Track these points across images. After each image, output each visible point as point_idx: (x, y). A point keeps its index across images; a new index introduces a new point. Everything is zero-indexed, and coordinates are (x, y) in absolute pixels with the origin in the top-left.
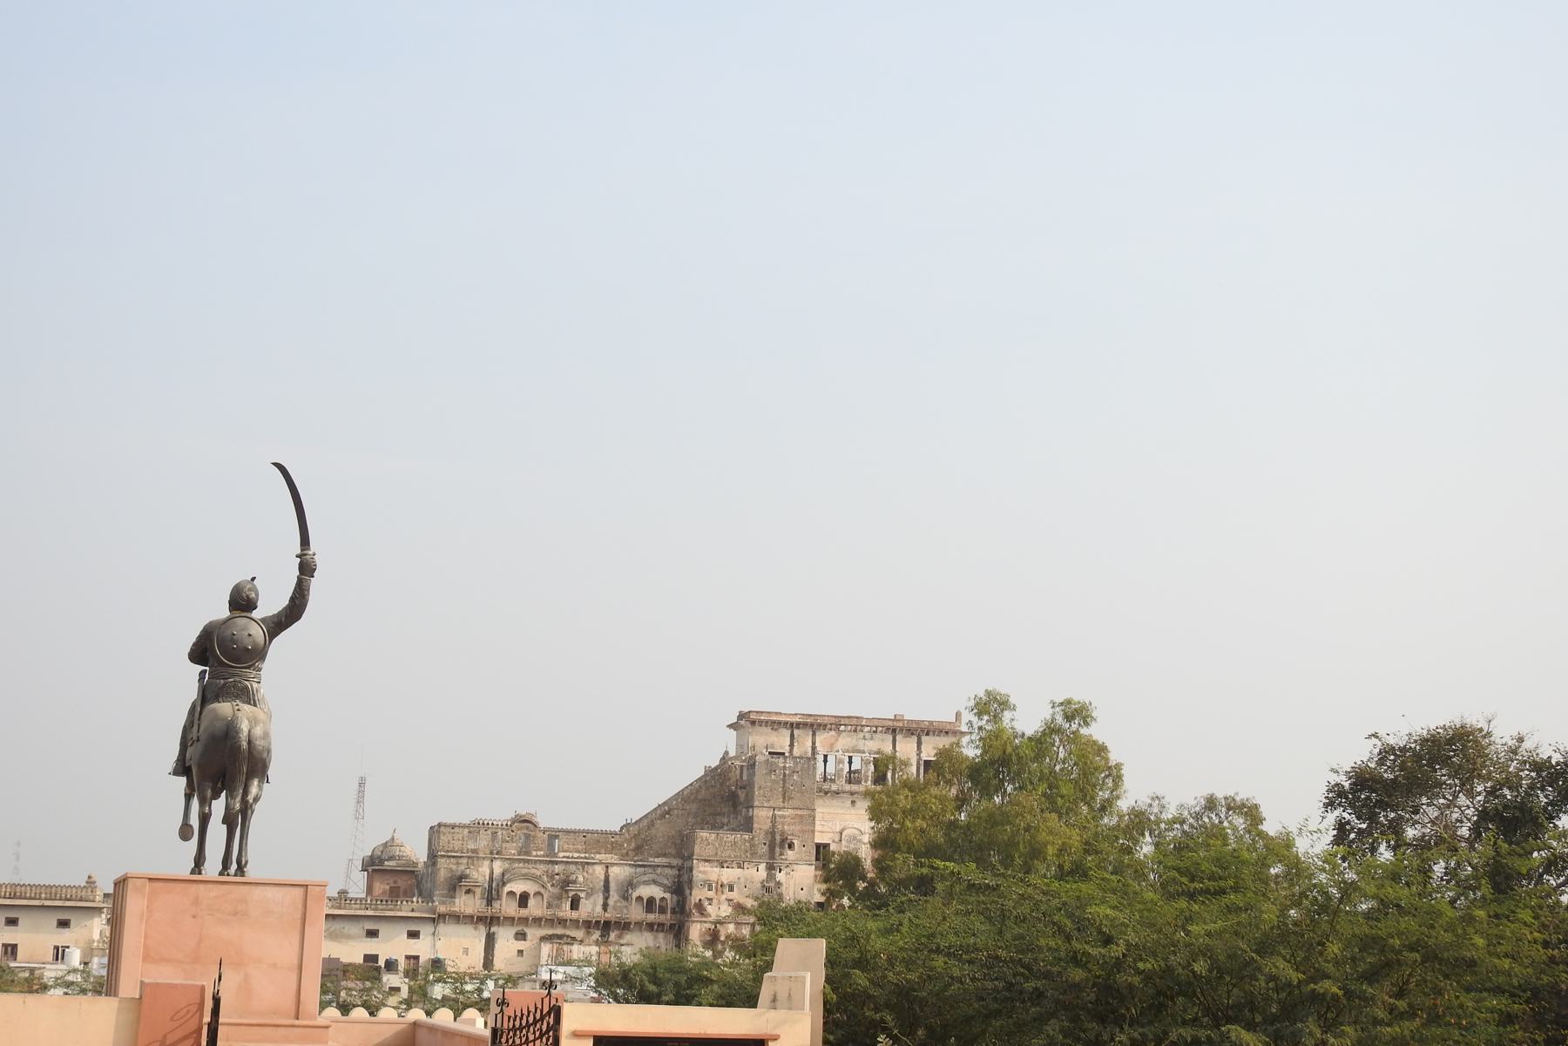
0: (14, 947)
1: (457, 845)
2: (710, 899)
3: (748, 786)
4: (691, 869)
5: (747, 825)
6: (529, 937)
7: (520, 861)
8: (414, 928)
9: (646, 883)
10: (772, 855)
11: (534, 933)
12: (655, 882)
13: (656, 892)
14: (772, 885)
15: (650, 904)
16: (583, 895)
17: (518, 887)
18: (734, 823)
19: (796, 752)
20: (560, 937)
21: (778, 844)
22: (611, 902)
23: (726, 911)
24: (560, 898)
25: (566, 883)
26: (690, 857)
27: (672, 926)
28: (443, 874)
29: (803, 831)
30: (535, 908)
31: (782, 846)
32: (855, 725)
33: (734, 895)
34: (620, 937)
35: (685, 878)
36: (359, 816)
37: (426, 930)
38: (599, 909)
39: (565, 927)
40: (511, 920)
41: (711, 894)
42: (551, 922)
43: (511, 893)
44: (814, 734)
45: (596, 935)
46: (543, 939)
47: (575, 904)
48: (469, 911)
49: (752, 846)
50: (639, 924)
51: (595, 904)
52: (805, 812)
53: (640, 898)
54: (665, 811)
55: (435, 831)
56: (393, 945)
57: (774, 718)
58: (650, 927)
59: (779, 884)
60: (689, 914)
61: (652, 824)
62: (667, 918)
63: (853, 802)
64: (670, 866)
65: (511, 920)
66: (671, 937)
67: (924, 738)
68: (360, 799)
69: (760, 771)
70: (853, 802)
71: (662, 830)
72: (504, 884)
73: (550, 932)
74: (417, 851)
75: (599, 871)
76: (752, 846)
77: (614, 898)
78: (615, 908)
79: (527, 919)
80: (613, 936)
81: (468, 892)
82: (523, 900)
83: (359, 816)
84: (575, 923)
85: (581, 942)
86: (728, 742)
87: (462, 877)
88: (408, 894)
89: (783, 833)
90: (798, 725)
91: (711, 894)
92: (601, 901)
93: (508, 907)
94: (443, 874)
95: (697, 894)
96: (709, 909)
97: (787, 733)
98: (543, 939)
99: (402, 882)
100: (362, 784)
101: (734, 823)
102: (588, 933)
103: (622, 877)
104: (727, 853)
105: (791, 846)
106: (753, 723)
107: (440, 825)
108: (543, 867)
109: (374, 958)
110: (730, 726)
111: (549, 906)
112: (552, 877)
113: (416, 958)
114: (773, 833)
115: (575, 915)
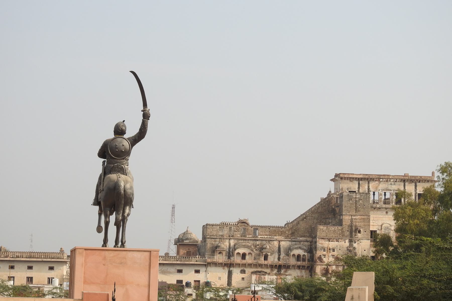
0: (32, 278)
1: (215, 233)
2: (325, 255)
3: (340, 206)
4: (316, 242)
5: (340, 223)
6: (247, 272)
8: (197, 268)
11: (249, 270)
12: (300, 248)
13: (300, 252)
14: (352, 249)
16: (269, 254)
18: (334, 222)
19: (361, 191)
20: (260, 272)
21: (354, 231)
22: (281, 257)
23: (331, 259)
24: (259, 255)
25: (262, 249)
26: (315, 237)
27: (308, 267)
29: (365, 225)
30: (249, 259)
31: (355, 232)
32: (387, 178)
33: (335, 253)
34: (286, 272)
36: (172, 221)
37: (202, 269)
38: (276, 260)
39: (262, 268)
40: (239, 265)
42: (256, 265)
43: (238, 254)
44: (369, 183)
45: (275, 271)
46: (253, 273)
47: (266, 258)
48: (220, 261)
49: (343, 232)
50: (294, 266)
51: (274, 258)
52: (366, 217)
53: (294, 255)
54: (304, 217)
55: (205, 227)
57: (351, 176)
58: (299, 267)
59: (355, 248)
60: (316, 262)
61: (298, 223)
62: (306, 263)
63: (387, 212)
64: (307, 241)
65: (239, 265)
67: (418, 184)
69: (345, 199)
70: (387, 212)
71: (303, 226)
72: (235, 250)
73: (256, 270)
74: (198, 236)
75: (276, 243)
76: (343, 232)
78: (283, 259)
79: (245, 264)
80: (282, 271)
81: (220, 253)
82: (244, 256)
83: (172, 221)
84: (266, 266)
85: (269, 274)
86: (331, 187)
87: (217, 247)
88: (194, 254)
89: (356, 226)
90: (361, 179)
92: (277, 256)
93: (238, 260)
94: (209, 246)
95: (319, 253)
97: (357, 182)
98: (253, 273)
99: (192, 249)
100: (173, 208)
101: (334, 222)
102: (272, 270)
103: (286, 246)
104: (332, 235)
105: (359, 232)
106: (342, 178)
107: (207, 225)
110: (332, 180)
112: (256, 246)
113: (199, 281)
114: (351, 226)
115: (266, 262)
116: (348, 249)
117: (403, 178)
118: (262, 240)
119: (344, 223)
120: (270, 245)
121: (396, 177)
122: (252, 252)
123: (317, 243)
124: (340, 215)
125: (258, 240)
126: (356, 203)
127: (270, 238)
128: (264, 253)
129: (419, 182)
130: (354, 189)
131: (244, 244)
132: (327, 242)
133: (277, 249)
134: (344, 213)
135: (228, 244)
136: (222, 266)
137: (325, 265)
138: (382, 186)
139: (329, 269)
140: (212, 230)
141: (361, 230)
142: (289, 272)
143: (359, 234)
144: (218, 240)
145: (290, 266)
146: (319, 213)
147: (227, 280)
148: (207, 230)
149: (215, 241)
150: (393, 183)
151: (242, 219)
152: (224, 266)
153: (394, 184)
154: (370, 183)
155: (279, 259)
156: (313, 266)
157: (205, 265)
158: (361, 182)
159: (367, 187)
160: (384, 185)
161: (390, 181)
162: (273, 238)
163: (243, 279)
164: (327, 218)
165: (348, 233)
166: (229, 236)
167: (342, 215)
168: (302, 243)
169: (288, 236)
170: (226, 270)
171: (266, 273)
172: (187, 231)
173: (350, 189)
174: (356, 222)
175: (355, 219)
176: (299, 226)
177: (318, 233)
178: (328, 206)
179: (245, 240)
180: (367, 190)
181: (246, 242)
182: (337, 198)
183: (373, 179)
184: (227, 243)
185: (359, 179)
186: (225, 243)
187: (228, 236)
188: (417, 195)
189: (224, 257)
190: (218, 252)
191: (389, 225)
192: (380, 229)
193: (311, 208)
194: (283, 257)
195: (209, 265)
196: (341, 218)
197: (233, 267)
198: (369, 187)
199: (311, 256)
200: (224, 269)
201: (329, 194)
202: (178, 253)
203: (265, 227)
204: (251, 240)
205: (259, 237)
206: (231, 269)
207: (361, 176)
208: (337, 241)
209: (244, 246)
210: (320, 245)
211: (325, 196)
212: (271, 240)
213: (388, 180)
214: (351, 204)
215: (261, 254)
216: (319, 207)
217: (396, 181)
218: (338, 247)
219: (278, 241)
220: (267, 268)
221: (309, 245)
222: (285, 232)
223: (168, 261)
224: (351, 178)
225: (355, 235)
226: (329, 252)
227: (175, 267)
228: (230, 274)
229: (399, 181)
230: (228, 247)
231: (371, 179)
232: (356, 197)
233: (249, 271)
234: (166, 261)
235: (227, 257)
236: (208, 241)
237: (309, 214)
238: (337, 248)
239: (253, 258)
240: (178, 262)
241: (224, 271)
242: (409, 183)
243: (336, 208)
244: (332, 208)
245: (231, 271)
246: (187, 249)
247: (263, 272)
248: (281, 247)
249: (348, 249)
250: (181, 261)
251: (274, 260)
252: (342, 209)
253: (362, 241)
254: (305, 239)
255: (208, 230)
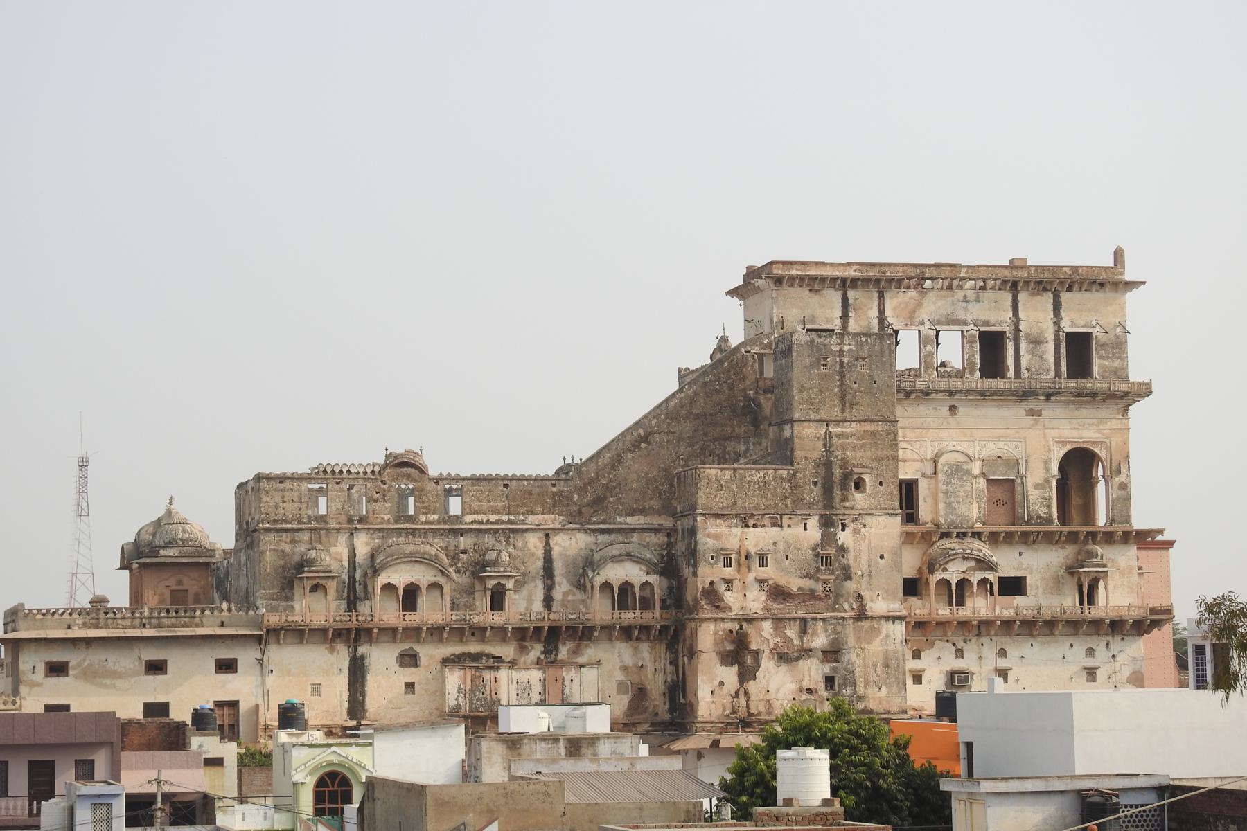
0: (413, 684)
1: (290, 509)
2: (729, 582)
3: (779, 389)
4: (693, 532)
5: (783, 453)
6: (423, 660)
7: (398, 531)
8: (226, 654)
9: (617, 559)
10: (828, 502)
11: (430, 653)
12: (630, 556)
13: (634, 573)
14: (831, 551)
15: (624, 595)
16: (510, 584)
17: (400, 576)
18: (756, 452)
19: (853, 326)
20: (476, 657)
21: (836, 483)
22: (557, 594)
23: (756, 601)
24: (470, 591)
25: (479, 567)
26: (691, 510)
27: (664, 629)
28: (269, 560)
29: (878, 459)
30: (430, 611)
31: (844, 487)
32: (947, 277)
33: (770, 572)
34: (576, 652)
35: (681, 547)
36: (81, 512)
37: (246, 657)
38: (538, 607)
39: (483, 640)
40: (391, 633)
41: (729, 572)
42: (458, 632)
43: (390, 588)
44: (881, 297)
45: (536, 651)
46: (447, 662)
47: (497, 603)
48: (319, 620)
49: (795, 487)
50: (608, 629)
51: (530, 600)
52: (880, 427)
53: (606, 586)
54: (639, 438)
55: (248, 493)
56: (190, 688)
57: (813, 272)
58: (627, 633)
59: (842, 550)
60: (695, 608)
61: (618, 460)
62: (653, 617)
63: (953, 409)
64: (656, 531)
65: (391, 633)
66: (661, 648)
67: (1065, 296)
68: (82, 488)
69: (801, 359)
70: (953, 409)
71: (635, 469)
72: (376, 572)
73: (458, 649)
74: (217, 530)
75: (534, 543)
76: (795, 487)
77: (562, 587)
78: (564, 604)
79: (417, 630)
80: (564, 652)
81: (315, 588)
82: (410, 597)
83: (81, 512)
84: (501, 633)
85: (513, 664)
86: (732, 323)
87: (303, 564)
88: (204, 600)
89: (844, 463)
90: (855, 282)
91: (729, 572)
92: (539, 593)
93: (387, 612)
94: (269, 560)
95: (708, 573)
96: (729, 598)
97: (835, 297)
98: (447, 662)
99: (191, 583)
100: (83, 466)
101: (756, 452)
102: (523, 649)
103: (572, 552)
104: (754, 501)
105: (859, 485)
106: (779, 281)
107: (259, 478)
108: (438, 542)
109: (163, 709)
110: (733, 293)
111: (454, 606)
112: (455, 557)
113: (234, 705)
114: (828, 465)
115: (498, 619)
116: (817, 555)
117: (1007, 273)
118: (479, 531)
119: (798, 453)
120: (511, 550)
121: (984, 274)
122: (441, 580)
123: (700, 536)
124: (780, 425)
125: (462, 533)
126: (842, 375)
127: (510, 522)
128: (490, 584)
129: (1070, 289)
130: (828, 322)
131: (410, 548)
132: (737, 531)
133: (540, 563)
134: (797, 415)
135: (345, 553)
136: (325, 641)
137: (732, 620)
138: (933, 305)
139: (746, 635)
140: (278, 500)
141: (866, 477)
142: (590, 652)
143: (858, 496)
144: (305, 536)
145: (592, 629)
146: (697, 417)
147: (346, 694)
148: (259, 500)
149: (294, 542)
150: (971, 295)
151: (398, 449)
152: (333, 640)
153: (977, 300)
154: (887, 295)
155: (548, 602)
156: (683, 627)
157: (258, 639)
158: (851, 294)
159: (874, 313)
160: (940, 303)
161: (961, 288)
162: (522, 522)
163: (410, 686)
164: (729, 439)
165: (813, 493)
166: (350, 521)
167: (791, 422)
168: (635, 537)
169: (580, 512)
170: (341, 658)
171: (499, 659)
172: (169, 513)
173: (813, 321)
174: (844, 447)
175: (842, 435)
176: (621, 471)
177: (700, 493)
178: (731, 388)
179: (413, 532)
180: (875, 323)
181: (418, 540)
182: (761, 356)
183: (896, 283)
184: (341, 549)
185: (844, 281)
186: (333, 550)
187: (343, 518)
188: (1063, 336)
189: (333, 605)
190: (308, 584)
191: (962, 458)
192: (929, 472)
193: (667, 400)
194: (565, 594)
195: (272, 639)
196: (787, 432)
197: (370, 641)
198: (882, 311)
199: (670, 588)
200: (332, 650)
201: (719, 349)
202: (136, 597)
203: (488, 479)
204: (435, 531)
205: (469, 518)
206: (362, 650)
207: (851, 273)
208: (774, 525)
209: (411, 555)
210: (710, 541)
211: (700, 358)
212: (514, 531)
213: (955, 283)
214: (825, 377)
215: (478, 587)
216: (696, 394)
217: (983, 288)
218: (781, 546)
219: (541, 534)
220: (504, 640)
221: (661, 546)
222: (569, 498)
223: (106, 627)
224: (814, 279)
225: (844, 499)
226: (744, 569)
227: (136, 653)
228: (357, 672)
229: (993, 288)
230: (346, 564)
231: (890, 280)
232: (841, 351)
233: (432, 657)
234: (97, 627)
235: (344, 605)
236: (267, 543)
237: (658, 425)
238: (776, 552)
239: (448, 603)
240: (149, 632)
241: (332, 658)
242: (1033, 295)
243: (762, 399)
244: (748, 399)
245: (363, 657)
246: (172, 582)
247: (488, 656)
248: (555, 554)
249: (817, 555)
250: (159, 626)
251: (529, 609)
252: (791, 397)
253: (868, 520)
254: (647, 519)
255: (264, 498)
